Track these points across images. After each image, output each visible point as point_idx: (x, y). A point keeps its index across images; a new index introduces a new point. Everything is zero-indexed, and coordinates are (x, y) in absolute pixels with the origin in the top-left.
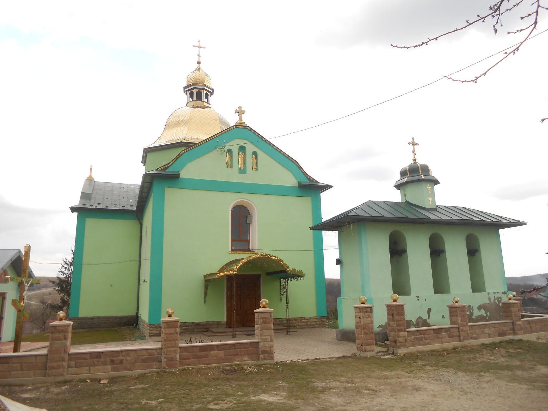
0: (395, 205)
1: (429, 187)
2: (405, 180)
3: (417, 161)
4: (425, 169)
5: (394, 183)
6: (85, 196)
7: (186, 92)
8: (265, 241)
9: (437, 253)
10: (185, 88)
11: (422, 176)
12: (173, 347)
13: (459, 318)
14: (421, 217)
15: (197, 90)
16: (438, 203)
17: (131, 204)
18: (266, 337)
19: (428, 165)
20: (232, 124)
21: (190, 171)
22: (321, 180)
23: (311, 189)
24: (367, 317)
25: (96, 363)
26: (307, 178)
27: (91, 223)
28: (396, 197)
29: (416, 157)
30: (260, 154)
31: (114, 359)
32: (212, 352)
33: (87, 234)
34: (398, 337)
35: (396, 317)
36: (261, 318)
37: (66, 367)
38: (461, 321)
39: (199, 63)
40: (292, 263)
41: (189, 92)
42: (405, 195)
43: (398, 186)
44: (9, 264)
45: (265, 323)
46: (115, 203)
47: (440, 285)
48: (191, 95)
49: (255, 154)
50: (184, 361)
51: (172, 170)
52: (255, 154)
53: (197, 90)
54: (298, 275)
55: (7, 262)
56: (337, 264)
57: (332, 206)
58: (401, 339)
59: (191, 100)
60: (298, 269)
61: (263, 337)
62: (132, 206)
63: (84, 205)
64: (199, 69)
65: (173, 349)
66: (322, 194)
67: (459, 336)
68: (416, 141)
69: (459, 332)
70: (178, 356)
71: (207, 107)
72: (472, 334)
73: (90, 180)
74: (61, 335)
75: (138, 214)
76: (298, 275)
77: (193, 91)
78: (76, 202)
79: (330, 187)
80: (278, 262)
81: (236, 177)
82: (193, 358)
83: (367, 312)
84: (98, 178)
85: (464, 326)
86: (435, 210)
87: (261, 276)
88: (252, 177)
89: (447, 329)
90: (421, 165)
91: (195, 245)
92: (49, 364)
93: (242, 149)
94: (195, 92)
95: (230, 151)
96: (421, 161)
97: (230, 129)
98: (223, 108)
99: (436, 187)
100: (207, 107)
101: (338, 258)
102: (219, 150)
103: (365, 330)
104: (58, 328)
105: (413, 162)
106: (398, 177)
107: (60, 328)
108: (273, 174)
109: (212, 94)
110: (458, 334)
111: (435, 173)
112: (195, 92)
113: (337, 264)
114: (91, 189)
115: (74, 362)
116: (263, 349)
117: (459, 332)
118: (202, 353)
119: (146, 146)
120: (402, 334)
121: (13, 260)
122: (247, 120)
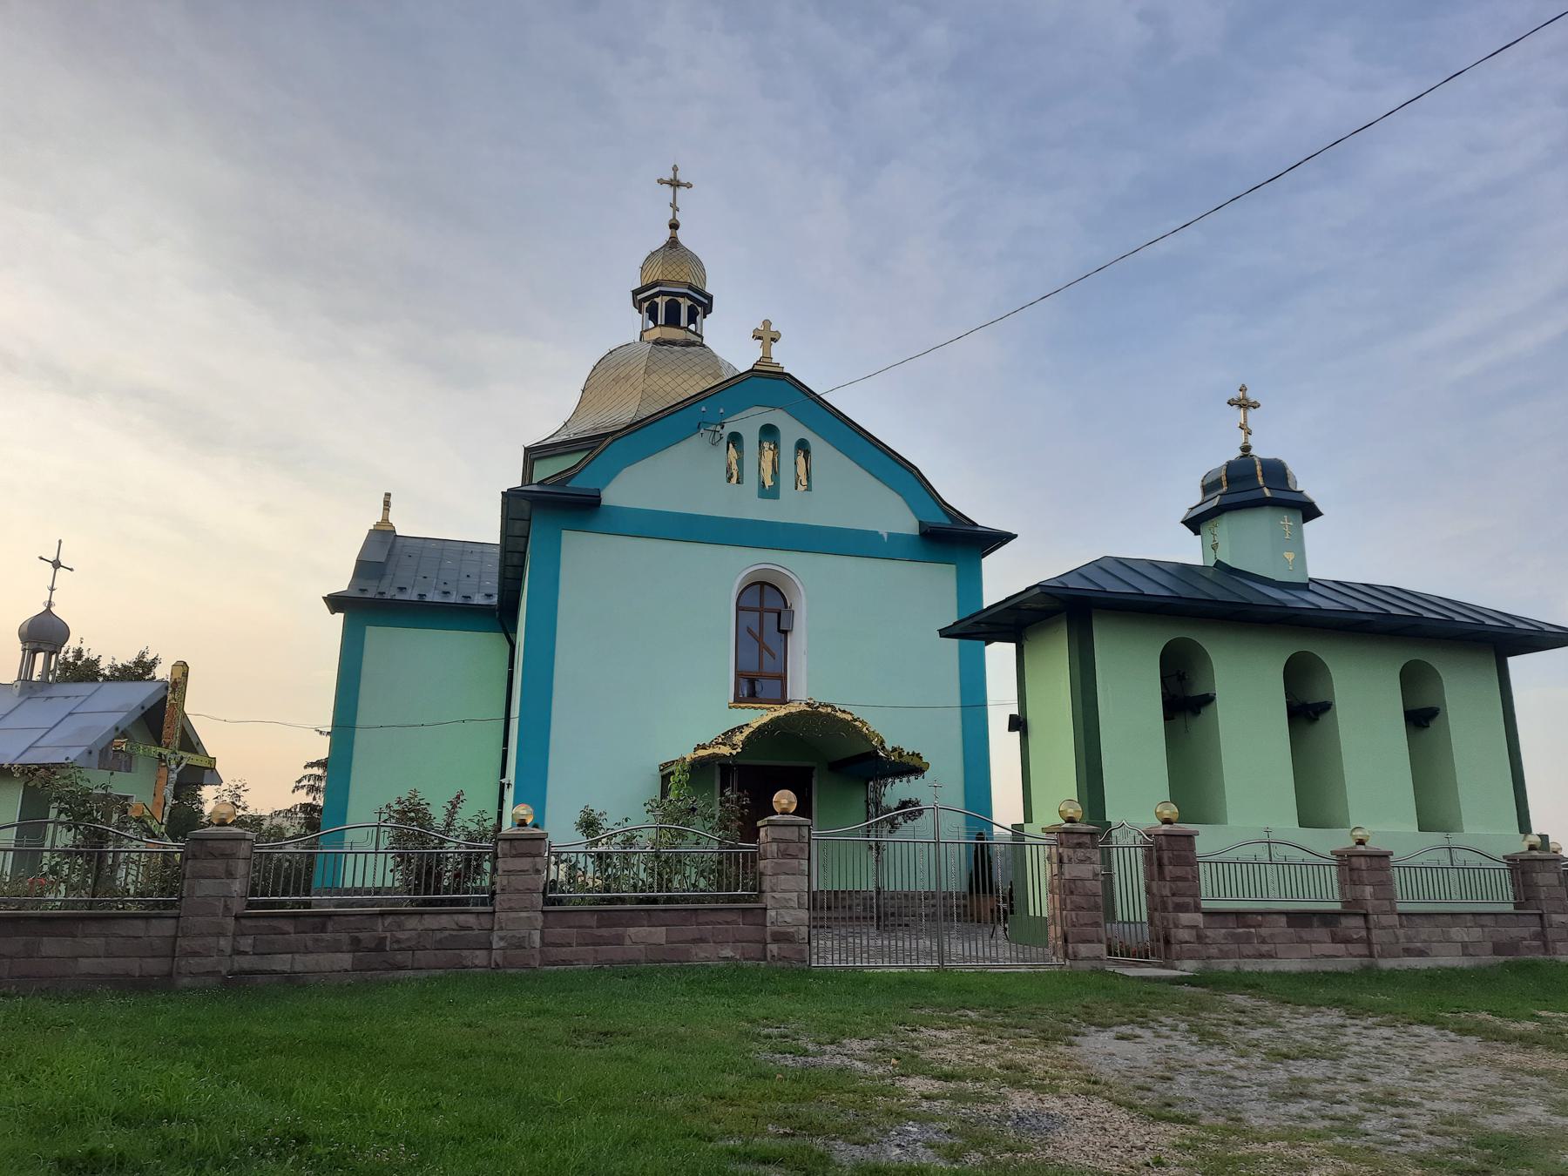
0: (1185, 571)
1: (1286, 520)
2: (1215, 502)
3: (1252, 452)
4: (1277, 472)
5: (1183, 513)
6: (364, 568)
7: (638, 304)
8: (822, 674)
9: (1307, 711)
10: (635, 293)
11: (1266, 490)
12: (524, 909)
13: (1369, 890)
14: (1255, 600)
15: (667, 298)
16: (1313, 573)
17: (485, 591)
18: (787, 895)
19: (1285, 460)
20: (743, 366)
21: (626, 490)
22: (985, 518)
23: (958, 541)
24: (1081, 861)
25: (310, 943)
26: (945, 512)
27: (378, 637)
28: (1189, 550)
29: (1251, 440)
30: (817, 445)
31: (360, 935)
32: (632, 930)
33: (367, 667)
34: (1176, 926)
35: (1168, 869)
36: (774, 840)
37: (229, 951)
38: (1375, 896)
39: (674, 226)
40: (892, 731)
41: (646, 305)
42: (1214, 547)
43: (1195, 523)
44: (139, 713)
45: (785, 855)
46: (446, 588)
47: (1315, 799)
48: (653, 316)
49: (803, 446)
50: (554, 950)
51: (579, 484)
52: (803, 446)
53: (667, 298)
54: (910, 767)
55: (130, 713)
56: (1010, 729)
57: (1001, 579)
58: (1184, 934)
59: (651, 324)
60: (908, 749)
61: (777, 895)
62: (489, 596)
63: (363, 591)
64: (673, 243)
65: (524, 914)
66: (987, 562)
67: (1368, 942)
68: (1252, 396)
69: (1368, 929)
70: (536, 936)
71: (693, 344)
72: (1410, 940)
73: (383, 535)
74: (219, 865)
75: (502, 616)
76: (910, 767)
77: (658, 300)
78: (341, 582)
79: (1015, 536)
80: (850, 729)
81: (749, 507)
82: (579, 945)
83: (1080, 845)
84: (405, 526)
85: (1385, 913)
86: (1304, 587)
87: (815, 773)
88: (789, 509)
89: (1328, 918)
90: (1263, 462)
91: (641, 693)
92: (182, 943)
93: (769, 432)
94: (661, 302)
95: (735, 439)
96: (1262, 451)
97: (740, 379)
98: (729, 342)
99: (1309, 527)
100: (693, 344)
101: (1016, 712)
102: (708, 435)
103: (1074, 897)
104: (210, 844)
105: (1240, 453)
106: (1197, 497)
107: (216, 844)
108: (845, 497)
109: (708, 309)
110: (1364, 933)
111: (1306, 483)
112: (661, 302)
113: (1010, 729)
114: (384, 551)
115: (250, 940)
116: (776, 928)
117: (1368, 929)
118: (604, 932)
119: (531, 441)
120: (1185, 918)
121: (148, 706)
122: (787, 358)
